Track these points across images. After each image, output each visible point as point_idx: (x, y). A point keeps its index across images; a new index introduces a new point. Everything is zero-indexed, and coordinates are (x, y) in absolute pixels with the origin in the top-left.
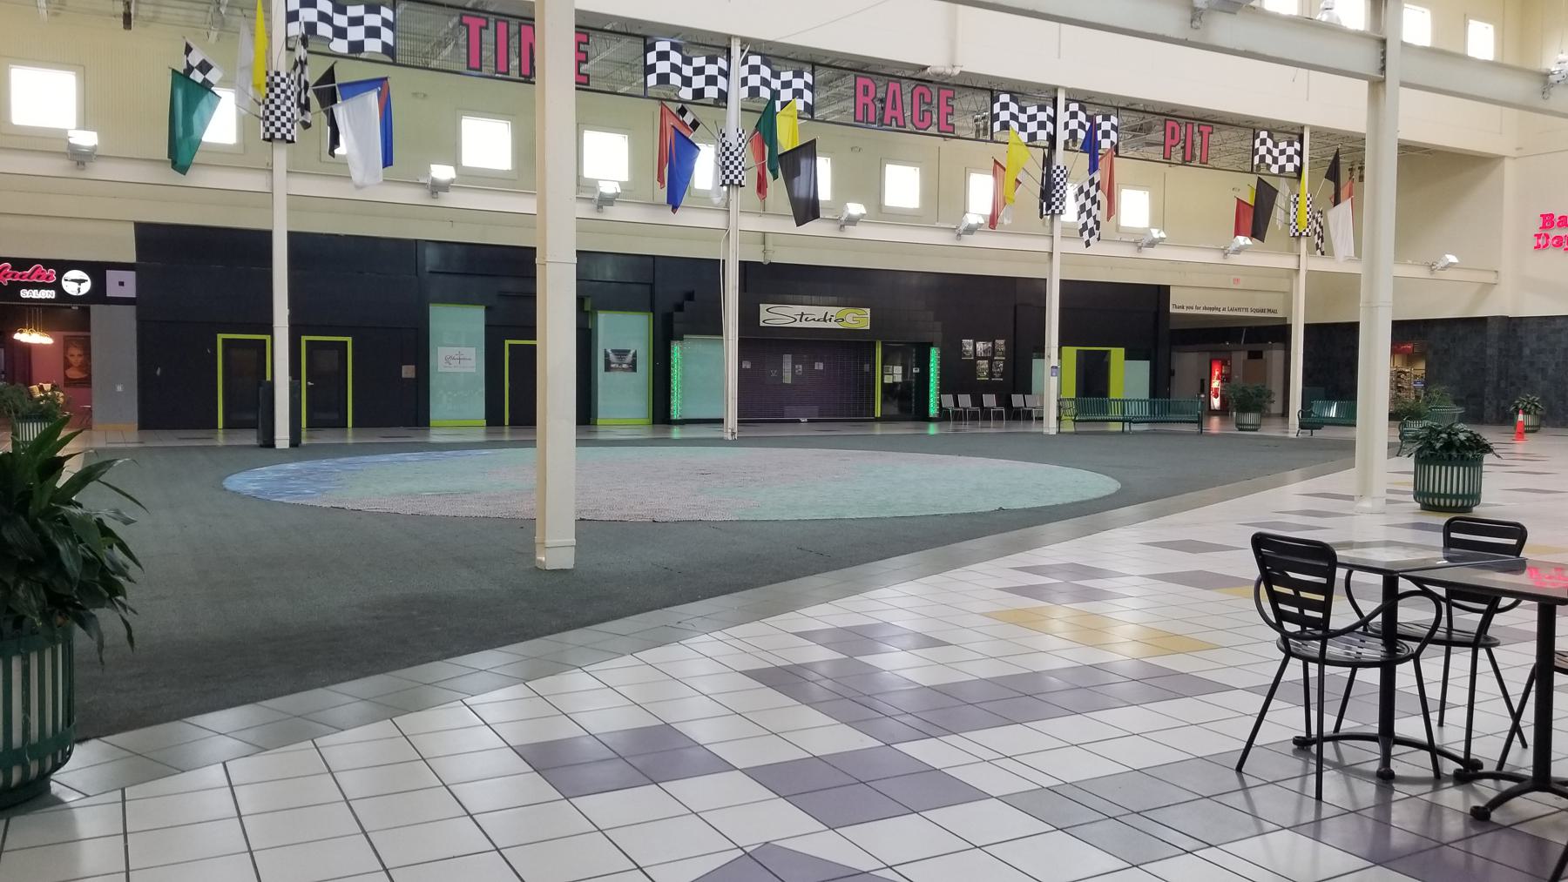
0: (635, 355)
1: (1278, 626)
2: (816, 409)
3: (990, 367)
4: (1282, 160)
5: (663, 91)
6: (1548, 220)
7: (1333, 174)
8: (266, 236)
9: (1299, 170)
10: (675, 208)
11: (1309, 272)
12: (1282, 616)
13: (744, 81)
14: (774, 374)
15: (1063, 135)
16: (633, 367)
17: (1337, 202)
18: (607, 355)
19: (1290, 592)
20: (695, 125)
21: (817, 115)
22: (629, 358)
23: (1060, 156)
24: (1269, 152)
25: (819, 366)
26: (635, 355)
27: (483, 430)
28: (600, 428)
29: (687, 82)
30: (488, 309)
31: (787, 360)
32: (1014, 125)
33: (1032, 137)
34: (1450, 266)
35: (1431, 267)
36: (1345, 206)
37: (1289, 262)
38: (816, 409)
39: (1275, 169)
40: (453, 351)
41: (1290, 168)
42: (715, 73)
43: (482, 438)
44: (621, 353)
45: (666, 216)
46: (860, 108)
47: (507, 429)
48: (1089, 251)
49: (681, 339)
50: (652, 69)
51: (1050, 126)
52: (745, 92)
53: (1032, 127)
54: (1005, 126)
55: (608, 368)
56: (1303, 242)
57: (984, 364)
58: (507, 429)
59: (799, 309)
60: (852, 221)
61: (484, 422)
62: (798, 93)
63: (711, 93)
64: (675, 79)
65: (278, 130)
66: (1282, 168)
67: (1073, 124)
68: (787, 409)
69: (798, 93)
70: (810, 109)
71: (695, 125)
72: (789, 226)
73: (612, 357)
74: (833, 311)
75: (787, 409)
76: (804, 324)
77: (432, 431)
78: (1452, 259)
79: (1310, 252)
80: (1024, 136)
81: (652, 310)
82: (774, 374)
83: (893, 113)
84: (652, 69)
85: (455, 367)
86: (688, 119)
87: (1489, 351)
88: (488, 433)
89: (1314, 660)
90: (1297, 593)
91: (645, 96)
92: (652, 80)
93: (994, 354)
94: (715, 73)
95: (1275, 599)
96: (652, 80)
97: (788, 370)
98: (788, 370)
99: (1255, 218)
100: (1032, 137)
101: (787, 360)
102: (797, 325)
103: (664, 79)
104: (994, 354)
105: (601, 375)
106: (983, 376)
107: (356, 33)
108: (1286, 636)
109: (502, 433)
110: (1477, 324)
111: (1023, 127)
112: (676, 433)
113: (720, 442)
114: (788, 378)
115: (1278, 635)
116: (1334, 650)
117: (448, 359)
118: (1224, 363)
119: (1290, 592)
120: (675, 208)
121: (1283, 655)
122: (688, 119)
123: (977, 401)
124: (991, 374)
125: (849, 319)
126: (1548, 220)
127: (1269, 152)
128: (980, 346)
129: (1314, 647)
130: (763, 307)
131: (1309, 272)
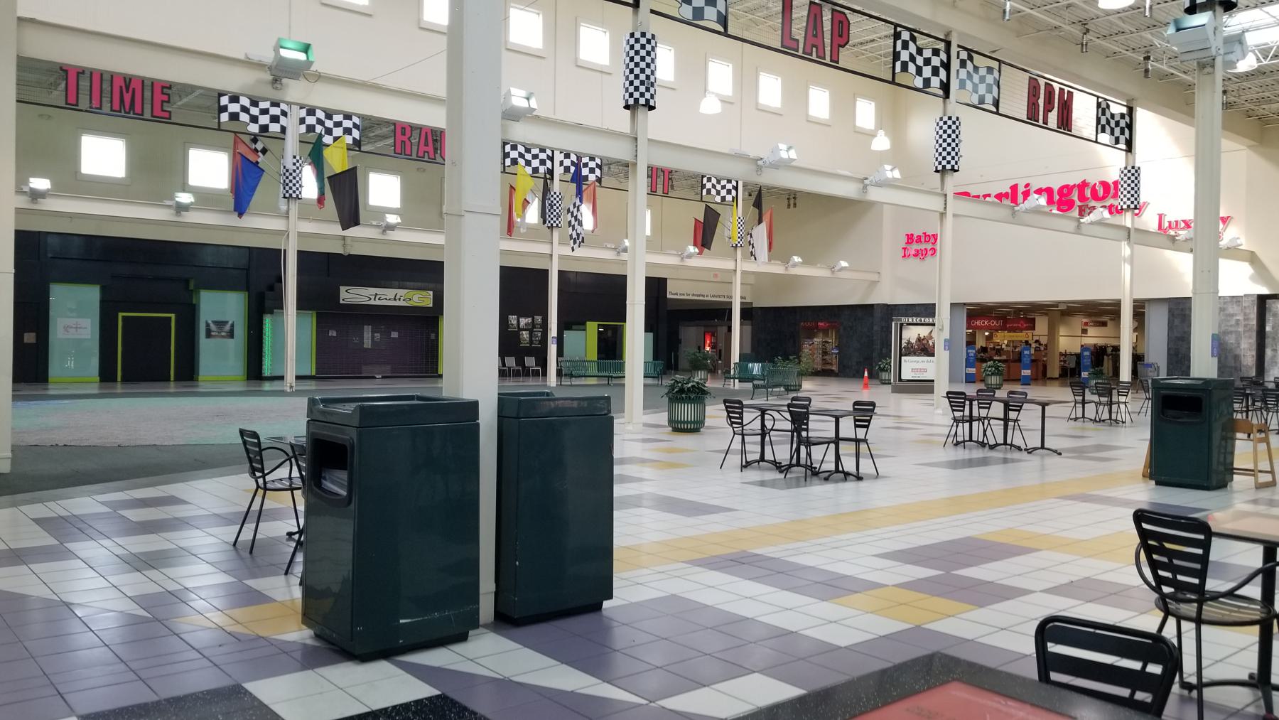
0: (232, 325)
1: (1157, 589)
2: (388, 368)
3: (531, 336)
4: (723, 193)
5: (234, 126)
6: (910, 238)
7: (758, 204)
8: (544, 274)
9: (736, 199)
10: (240, 215)
11: (744, 273)
12: (1160, 581)
13: (302, 121)
14: (356, 340)
15: (558, 171)
16: (231, 334)
17: (760, 222)
18: (208, 325)
19: (1165, 560)
20: (264, 151)
21: (363, 148)
22: (228, 327)
23: (556, 186)
24: (714, 186)
25: (395, 335)
26: (232, 325)
27: (97, 385)
28: (201, 384)
29: (254, 119)
30: (104, 291)
31: (367, 332)
32: (521, 161)
33: (536, 170)
34: (843, 269)
35: (832, 269)
36: (763, 227)
37: (729, 265)
38: (388, 368)
39: (718, 199)
40: (71, 321)
41: (729, 198)
42: (938, 64)
43: (96, 391)
44: (220, 324)
45: (233, 220)
46: (398, 145)
47: (119, 385)
48: (574, 254)
49: (272, 313)
50: (224, 109)
51: (549, 164)
52: (303, 129)
53: (535, 163)
54: (514, 162)
55: (209, 335)
56: (739, 251)
57: (525, 335)
58: (119, 385)
59: (372, 291)
60: (391, 227)
61: (98, 379)
62: (348, 131)
63: (274, 128)
64: (244, 117)
65: (642, 95)
66: (723, 199)
67: (567, 163)
68: (364, 368)
69: (348, 131)
70: (357, 143)
71: (264, 151)
72: (337, 229)
73: (213, 327)
74: (401, 292)
75: (364, 368)
76: (378, 303)
77: (50, 386)
78: (844, 264)
79: (744, 257)
80: (529, 170)
81: (248, 289)
82: (356, 340)
83: (426, 149)
84: (224, 109)
85: (73, 335)
86: (259, 146)
87: (876, 328)
88: (101, 388)
89: (1189, 619)
90: (1171, 561)
91: (219, 129)
92: (224, 117)
93: (534, 326)
94: (938, 64)
95: (1154, 566)
96: (224, 117)
97: (368, 337)
98: (368, 337)
99: (705, 234)
100: (536, 170)
101: (367, 332)
102: (372, 302)
103: (234, 116)
104: (534, 326)
105: (204, 344)
106: (525, 344)
107: (264, 120)
108: (1163, 597)
109: (115, 388)
110: (868, 309)
111: (528, 163)
112: (267, 386)
113: (282, 393)
114: (367, 343)
115: (1156, 595)
116: (1210, 610)
117: (67, 328)
118: (713, 335)
119: (1165, 560)
120: (240, 215)
121: (1162, 614)
122: (259, 146)
123: (520, 362)
124: (531, 342)
125: (415, 298)
126: (910, 238)
127: (714, 186)
128: (523, 321)
129: (1191, 609)
130: (343, 289)
131: (744, 273)
